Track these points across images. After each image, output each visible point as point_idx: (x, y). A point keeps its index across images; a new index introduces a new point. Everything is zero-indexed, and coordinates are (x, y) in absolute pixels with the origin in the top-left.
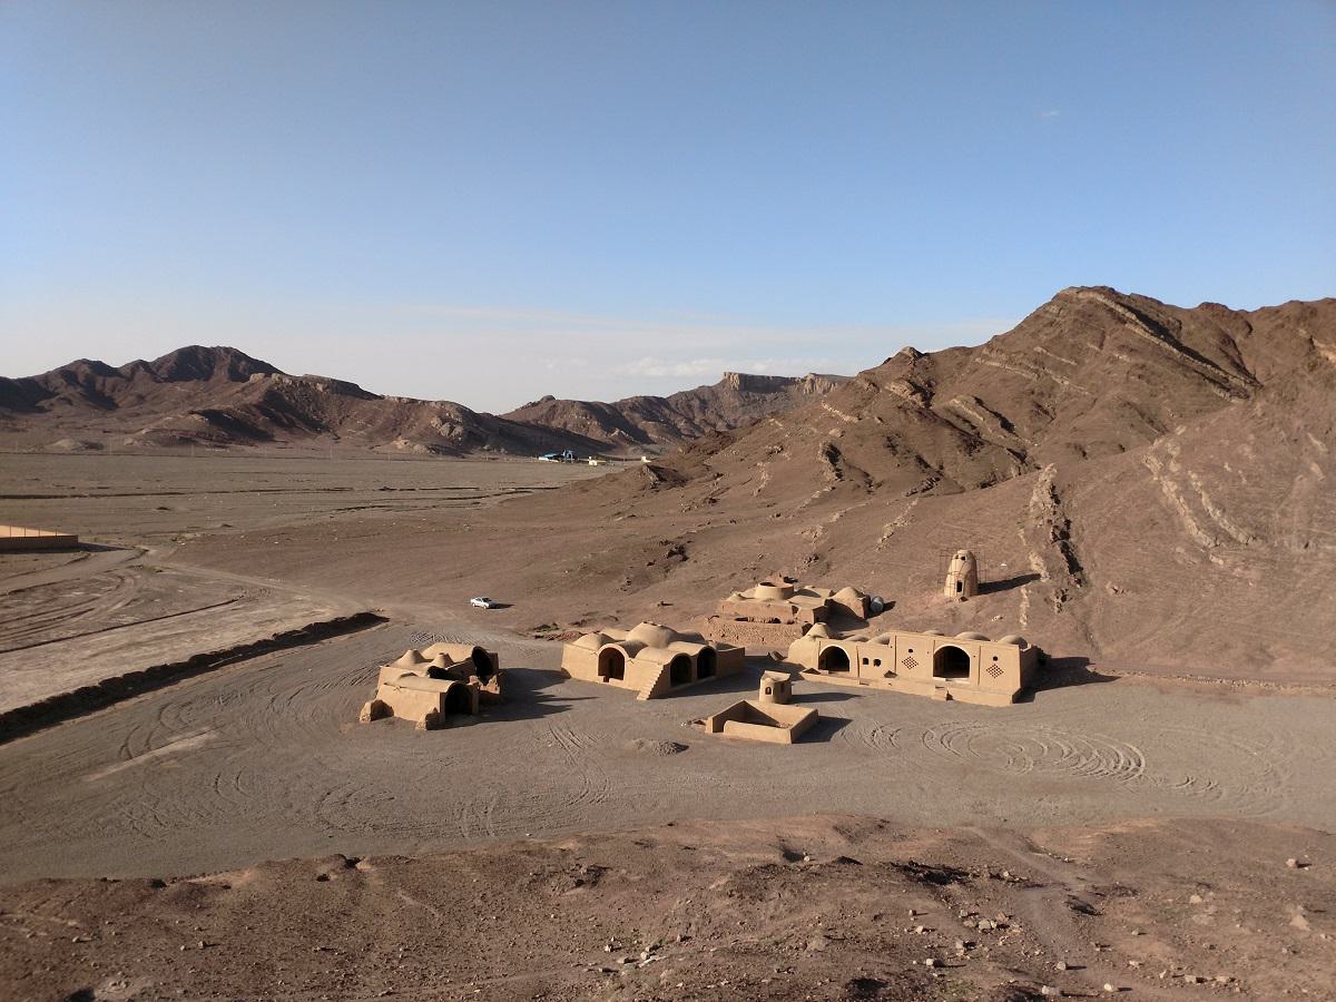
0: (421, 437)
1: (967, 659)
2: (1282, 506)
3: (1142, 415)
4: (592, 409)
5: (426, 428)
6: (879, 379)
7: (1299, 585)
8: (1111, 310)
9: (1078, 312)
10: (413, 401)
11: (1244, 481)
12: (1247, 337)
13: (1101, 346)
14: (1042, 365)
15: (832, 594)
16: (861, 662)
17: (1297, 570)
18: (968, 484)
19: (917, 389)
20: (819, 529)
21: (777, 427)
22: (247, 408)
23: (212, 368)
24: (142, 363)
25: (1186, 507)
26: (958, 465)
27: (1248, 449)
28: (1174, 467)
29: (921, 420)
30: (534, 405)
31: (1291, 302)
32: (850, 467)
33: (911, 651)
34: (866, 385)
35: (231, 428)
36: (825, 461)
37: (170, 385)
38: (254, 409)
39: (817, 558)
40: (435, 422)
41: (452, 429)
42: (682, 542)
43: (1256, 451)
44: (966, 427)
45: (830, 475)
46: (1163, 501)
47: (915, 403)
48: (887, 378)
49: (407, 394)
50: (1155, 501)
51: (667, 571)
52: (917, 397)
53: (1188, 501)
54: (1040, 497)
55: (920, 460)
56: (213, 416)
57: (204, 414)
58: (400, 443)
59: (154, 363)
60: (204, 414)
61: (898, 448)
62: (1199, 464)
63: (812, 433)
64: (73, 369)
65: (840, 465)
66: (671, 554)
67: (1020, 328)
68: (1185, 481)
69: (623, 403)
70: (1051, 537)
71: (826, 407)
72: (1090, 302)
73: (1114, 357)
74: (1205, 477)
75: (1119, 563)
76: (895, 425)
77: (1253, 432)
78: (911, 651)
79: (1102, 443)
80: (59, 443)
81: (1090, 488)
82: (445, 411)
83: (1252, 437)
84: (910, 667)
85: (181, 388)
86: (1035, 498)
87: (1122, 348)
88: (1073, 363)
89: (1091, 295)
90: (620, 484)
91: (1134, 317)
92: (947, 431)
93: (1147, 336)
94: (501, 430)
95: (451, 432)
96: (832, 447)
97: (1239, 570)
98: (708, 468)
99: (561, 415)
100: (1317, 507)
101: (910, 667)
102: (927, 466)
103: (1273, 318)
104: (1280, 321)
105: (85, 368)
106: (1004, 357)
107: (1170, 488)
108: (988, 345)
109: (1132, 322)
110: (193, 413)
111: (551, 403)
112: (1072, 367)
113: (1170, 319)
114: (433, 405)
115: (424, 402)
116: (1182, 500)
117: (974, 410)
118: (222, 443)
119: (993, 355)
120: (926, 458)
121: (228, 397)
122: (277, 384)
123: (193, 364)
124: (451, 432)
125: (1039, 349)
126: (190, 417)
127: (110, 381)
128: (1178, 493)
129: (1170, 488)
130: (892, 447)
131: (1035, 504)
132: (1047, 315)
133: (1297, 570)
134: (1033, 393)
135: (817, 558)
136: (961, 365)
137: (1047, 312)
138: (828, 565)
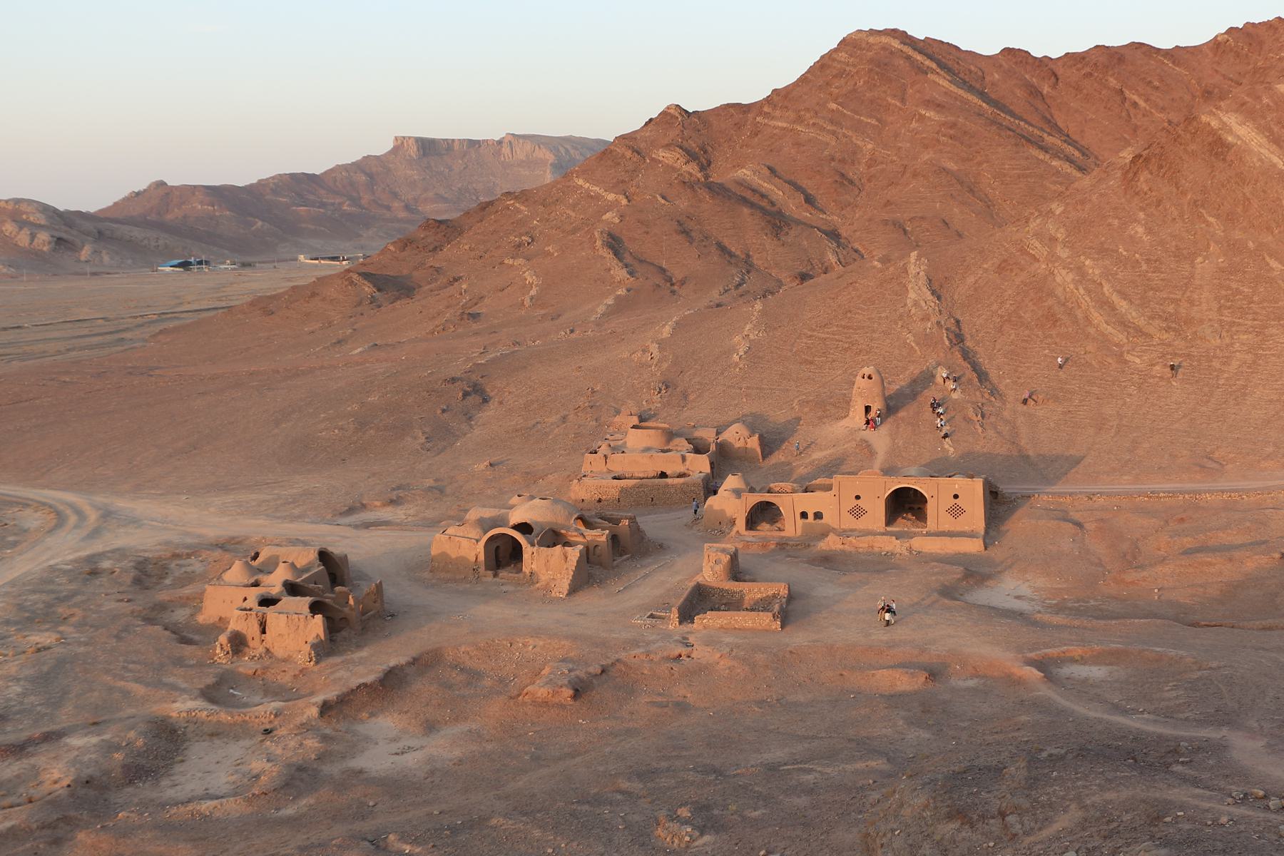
1: (923, 500)
2: (1188, 294)
3: (962, 183)
6: (643, 145)
7: (1221, 382)
8: (908, 58)
9: (871, 61)
11: (1144, 267)
12: (1054, 87)
13: (903, 100)
14: (838, 124)
16: (798, 516)
17: (1216, 364)
18: (784, 276)
19: (691, 156)
20: (654, 348)
21: (519, 211)
25: (1087, 299)
26: (765, 250)
27: (1140, 230)
28: (1063, 253)
29: (712, 198)
30: (138, 194)
31: (1097, 47)
32: (641, 261)
33: (858, 497)
34: (628, 154)
40: (9, 228)
41: (33, 236)
43: (1149, 231)
44: (764, 203)
45: (620, 273)
46: (1059, 292)
47: (691, 174)
50: (1051, 294)
51: (470, 419)
52: (693, 168)
53: (1089, 291)
54: (917, 293)
55: (722, 248)
61: (693, 234)
62: (1091, 248)
63: (569, 217)
67: (803, 79)
68: (1079, 268)
69: (262, 184)
70: (947, 343)
71: (581, 182)
72: (884, 48)
73: (920, 115)
74: (1100, 262)
75: (1029, 368)
77: (1142, 209)
78: (858, 497)
79: (922, 218)
81: (971, 280)
83: (1141, 215)
84: (858, 516)
86: (912, 295)
87: (929, 103)
88: (874, 122)
89: (884, 39)
90: (324, 300)
91: (934, 66)
92: (746, 211)
93: (953, 88)
94: (100, 232)
96: (610, 235)
97: (1157, 368)
98: (438, 270)
100: (1223, 292)
101: (858, 516)
102: (731, 255)
103: (1079, 66)
104: (1088, 70)
106: (791, 114)
107: (1064, 277)
108: (768, 100)
109: (933, 71)
112: (873, 126)
113: (973, 68)
116: (1082, 291)
117: (770, 182)
119: (778, 113)
125: (833, 106)
128: (1076, 283)
129: (1064, 277)
130: (686, 233)
131: (916, 304)
132: (835, 64)
133: (1216, 364)
134: (833, 159)
135: (667, 387)
136: (738, 126)
137: (834, 60)
138: (685, 396)
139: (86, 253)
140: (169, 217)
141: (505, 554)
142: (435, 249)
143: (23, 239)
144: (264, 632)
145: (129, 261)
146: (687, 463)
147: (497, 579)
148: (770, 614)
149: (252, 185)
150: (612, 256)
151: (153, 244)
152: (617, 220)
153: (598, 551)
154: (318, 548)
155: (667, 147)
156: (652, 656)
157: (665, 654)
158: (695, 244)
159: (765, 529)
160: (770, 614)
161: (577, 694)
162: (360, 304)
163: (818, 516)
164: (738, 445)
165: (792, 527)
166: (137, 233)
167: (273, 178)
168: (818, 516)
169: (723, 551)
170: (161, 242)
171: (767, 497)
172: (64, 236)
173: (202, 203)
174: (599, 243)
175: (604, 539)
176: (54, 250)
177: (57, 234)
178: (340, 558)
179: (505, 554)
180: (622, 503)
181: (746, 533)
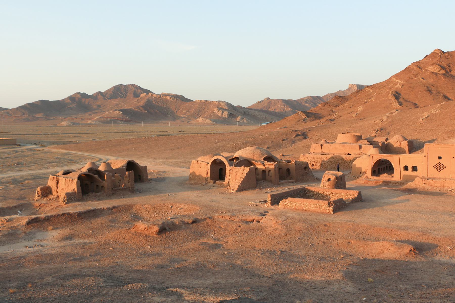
0: (209, 117)
4: (287, 102)
5: (212, 113)
10: (206, 101)
15: (387, 139)
19: (443, 68)
21: (369, 91)
22: (138, 107)
23: (127, 93)
24: (100, 93)
30: (261, 102)
32: (407, 101)
33: (440, 158)
34: (415, 68)
35: (131, 116)
36: (393, 99)
37: (110, 100)
38: (141, 108)
39: (381, 130)
40: (216, 110)
41: (223, 113)
42: (305, 131)
48: (427, 64)
49: (204, 98)
56: (124, 111)
57: (121, 110)
58: (200, 120)
59: (104, 92)
60: (121, 110)
61: (433, 92)
64: (74, 96)
65: (401, 100)
66: (297, 135)
69: (302, 99)
76: (431, 81)
78: (440, 158)
80: (62, 123)
82: (219, 105)
85: (114, 102)
95: (222, 114)
99: (273, 106)
105: (79, 96)
110: (116, 110)
111: (268, 101)
114: (215, 102)
115: (211, 101)
118: (127, 121)
120: (448, 95)
121: (132, 104)
122: (150, 97)
123: (119, 91)
124: (222, 114)
126: (115, 112)
127: (87, 100)
135: (381, 130)
139: (239, 118)
140: (270, 110)
141: (218, 172)
142: (336, 106)
143: (219, 113)
144: (58, 188)
145: (253, 122)
146: (362, 149)
147: (215, 185)
148: (326, 202)
149: (298, 100)
150: (394, 99)
151: (261, 117)
152: (400, 87)
153: (271, 174)
154: (128, 159)
155: (432, 65)
156: (234, 218)
157: (244, 218)
158: (433, 95)
159: (384, 177)
160: (326, 202)
161: (162, 230)
162: (299, 121)
163: (415, 169)
164: (395, 145)
165: (397, 177)
166: (257, 113)
167: (306, 97)
168: (415, 169)
169: (333, 174)
170: (264, 116)
171: (386, 157)
172: (232, 113)
173: (281, 105)
174: (390, 95)
175: (273, 167)
176: (229, 117)
177: (230, 112)
178: (142, 167)
179: (218, 172)
180: (324, 167)
181: (372, 177)
